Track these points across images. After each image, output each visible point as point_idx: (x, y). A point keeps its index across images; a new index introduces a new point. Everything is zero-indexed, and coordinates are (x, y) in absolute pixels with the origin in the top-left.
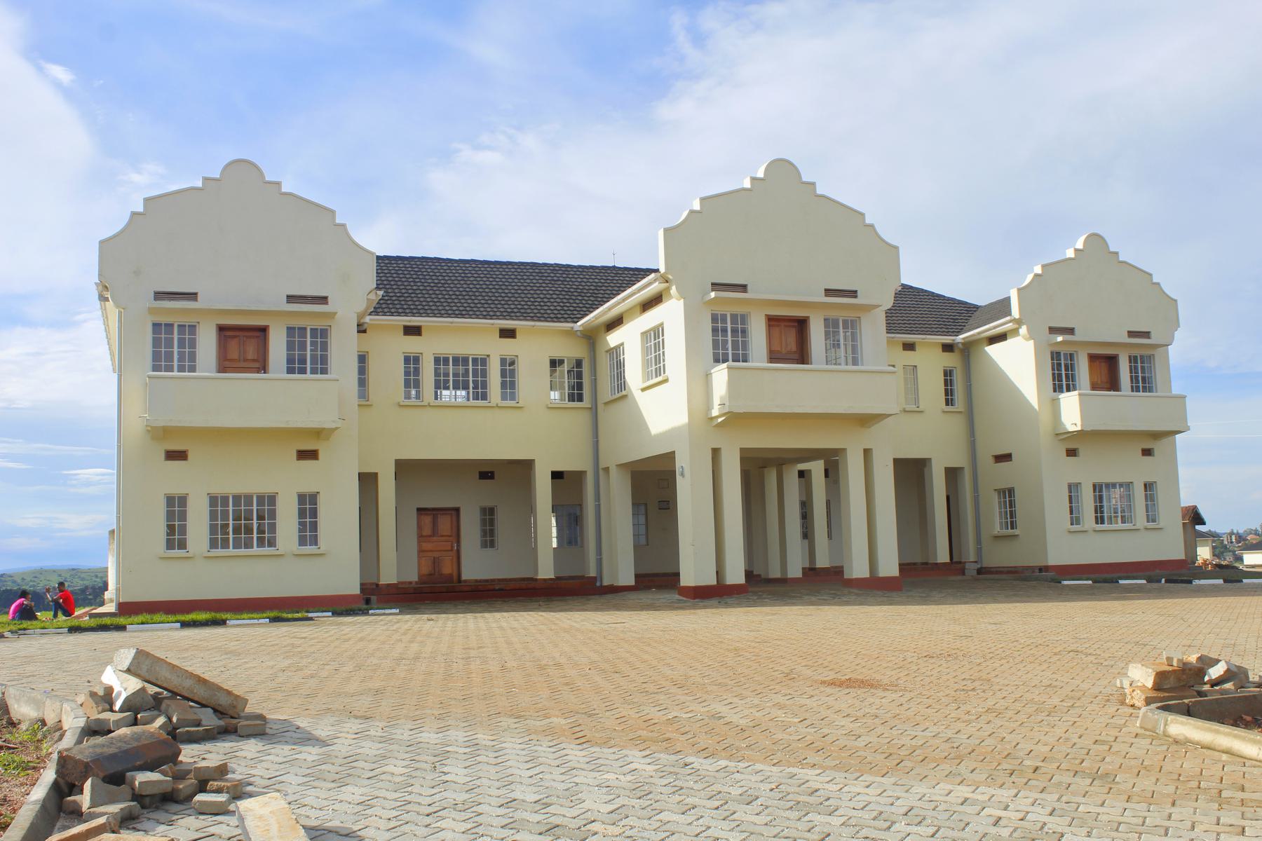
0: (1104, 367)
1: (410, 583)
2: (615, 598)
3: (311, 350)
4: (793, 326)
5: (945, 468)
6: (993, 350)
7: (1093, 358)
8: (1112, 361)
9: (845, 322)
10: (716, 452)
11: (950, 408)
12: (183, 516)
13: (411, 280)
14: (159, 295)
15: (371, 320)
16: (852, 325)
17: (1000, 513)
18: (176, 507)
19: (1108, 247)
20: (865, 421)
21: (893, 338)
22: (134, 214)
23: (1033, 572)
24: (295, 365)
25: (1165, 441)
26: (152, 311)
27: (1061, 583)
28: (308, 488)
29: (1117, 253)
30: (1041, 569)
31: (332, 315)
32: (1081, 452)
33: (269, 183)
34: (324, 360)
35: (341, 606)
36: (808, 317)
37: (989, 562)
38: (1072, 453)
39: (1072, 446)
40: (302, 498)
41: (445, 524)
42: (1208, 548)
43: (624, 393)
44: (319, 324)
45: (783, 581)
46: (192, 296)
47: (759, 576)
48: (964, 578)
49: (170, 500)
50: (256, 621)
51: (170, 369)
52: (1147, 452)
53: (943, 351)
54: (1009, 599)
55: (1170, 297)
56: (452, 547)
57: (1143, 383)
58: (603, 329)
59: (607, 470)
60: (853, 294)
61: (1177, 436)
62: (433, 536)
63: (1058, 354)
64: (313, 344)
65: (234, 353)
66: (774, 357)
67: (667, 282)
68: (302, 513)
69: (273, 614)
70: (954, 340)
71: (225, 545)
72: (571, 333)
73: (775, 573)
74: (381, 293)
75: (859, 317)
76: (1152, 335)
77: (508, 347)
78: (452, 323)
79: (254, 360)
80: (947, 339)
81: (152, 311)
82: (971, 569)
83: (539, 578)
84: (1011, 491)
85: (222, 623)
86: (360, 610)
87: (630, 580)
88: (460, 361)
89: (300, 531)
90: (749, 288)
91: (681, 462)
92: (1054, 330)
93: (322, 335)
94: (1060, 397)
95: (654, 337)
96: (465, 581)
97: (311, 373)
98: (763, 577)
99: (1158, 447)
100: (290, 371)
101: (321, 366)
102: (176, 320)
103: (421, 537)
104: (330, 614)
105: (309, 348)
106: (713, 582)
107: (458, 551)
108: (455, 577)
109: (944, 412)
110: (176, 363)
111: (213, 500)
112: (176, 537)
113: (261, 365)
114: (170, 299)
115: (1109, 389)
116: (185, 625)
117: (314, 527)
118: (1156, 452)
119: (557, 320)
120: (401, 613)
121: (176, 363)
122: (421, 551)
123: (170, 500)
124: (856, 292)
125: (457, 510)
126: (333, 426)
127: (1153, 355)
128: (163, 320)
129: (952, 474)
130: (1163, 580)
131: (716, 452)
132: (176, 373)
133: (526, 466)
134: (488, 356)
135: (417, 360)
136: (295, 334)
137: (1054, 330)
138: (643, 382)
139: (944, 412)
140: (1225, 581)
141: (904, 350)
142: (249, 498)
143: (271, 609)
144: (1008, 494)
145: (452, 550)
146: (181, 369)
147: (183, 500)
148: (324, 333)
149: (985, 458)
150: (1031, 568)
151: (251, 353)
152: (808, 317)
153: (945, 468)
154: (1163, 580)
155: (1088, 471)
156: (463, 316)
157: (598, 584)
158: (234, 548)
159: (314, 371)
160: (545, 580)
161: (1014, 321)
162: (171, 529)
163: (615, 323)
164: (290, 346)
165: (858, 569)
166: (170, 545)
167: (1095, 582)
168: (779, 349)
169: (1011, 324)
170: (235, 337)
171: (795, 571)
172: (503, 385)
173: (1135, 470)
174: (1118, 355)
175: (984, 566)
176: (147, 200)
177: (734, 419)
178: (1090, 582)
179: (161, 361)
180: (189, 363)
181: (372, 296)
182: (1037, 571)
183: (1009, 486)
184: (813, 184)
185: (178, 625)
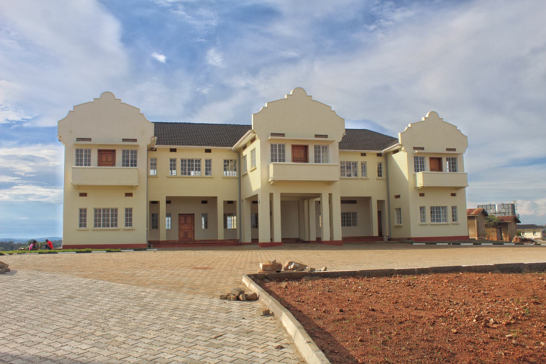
0: (437, 162)
1: (176, 241)
2: (246, 247)
3: (131, 158)
4: (303, 149)
5: (377, 200)
6: (395, 156)
7: (431, 159)
8: (439, 160)
9: (323, 147)
10: (271, 195)
11: (380, 178)
12: (85, 216)
13: (233, 131)
14: (78, 139)
15: (157, 147)
16: (325, 148)
17: (397, 217)
18: (83, 213)
19: (438, 116)
20: (329, 183)
21: (343, 151)
22: (70, 112)
23: (405, 240)
24: (126, 163)
25: (461, 190)
26: (75, 145)
27: (412, 244)
28: (129, 206)
29: (442, 119)
30: (408, 239)
31: (138, 146)
32: (425, 195)
33: (117, 99)
34: (136, 161)
35: (137, 248)
36: (308, 145)
37: (393, 236)
38: (422, 195)
39: (422, 193)
40: (127, 210)
41: (189, 220)
42: (540, 233)
43: (246, 173)
44: (134, 149)
45: (309, 242)
46: (90, 140)
47: (302, 240)
48: (383, 242)
49: (81, 210)
50: (101, 252)
51: (82, 165)
52: (453, 195)
53: (377, 156)
54: (364, 249)
55: (464, 135)
56: (192, 228)
57: (454, 168)
58: (242, 149)
59: (243, 200)
60: (326, 136)
61: (466, 188)
62: (185, 224)
63: (417, 157)
64: (131, 156)
65: (104, 159)
66: (295, 160)
67: (255, 133)
68: (127, 215)
69: (108, 249)
70: (381, 152)
71: (100, 226)
72: (231, 150)
73: (307, 240)
74: (156, 138)
75: (328, 145)
76: (457, 150)
77: (208, 156)
78: (187, 147)
79: (111, 162)
80: (378, 152)
81: (75, 145)
82: (386, 238)
83: (218, 239)
84: (400, 209)
85: (90, 252)
86: (144, 249)
87: (250, 241)
88: (349, 163)
89: (126, 221)
90: (285, 135)
91: (259, 198)
92: (415, 148)
93: (135, 153)
94: (417, 174)
95: (253, 151)
96: (196, 240)
97: (131, 166)
98: (304, 240)
99: (458, 193)
100: (123, 165)
101: (134, 164)
102: (84, 148)
103: (180, 224)
104: (133, 250)
105: (130, 157)
106: (269, 241)
107: (194, 229)
108: (193, 239)
109: (377, 179)
110: (130, 164)
111: (96, 210)
112: (83, 223)
113: (113, 164)
114: (82, 141)
115: (439, 171)
116: (77, 252)
117: (131, 220)
118: (457, 195)
119: (226, 146)
120: (158, 250)
121: (130, 164)
122: (180, 229)
123: (81, 210)
124: (327, 136)
125: (194, 214)
126: (136, 185)
127: (457, 157)
128: (80, 148)
129: (380, 203)
130: (451, 243)
131: (271, 195)
132: (83, 167)
133: (215, 199)
134: (201, 159)
135: (175, 160)
136: (125, 153)
137: (415, 148)
138: (251, 168)
139: (377, 179)
140: (493, 244)
141: (361, 156)
142: (108, 210)
143: (107, 248)
144: (399, 210)
145: (192, 229)
146: (86, 165)
147: (85, 210)
148: (136, 152)
149: (392, 197)
150: (405, 239)
151: (110, 159)
152: (308, 145)
153: (377, 200)
154: (451, 243)
155: (429, 202)
156: (191, 145)
157: (240, 242)
158: (103, 227)
159: (132, 166)
160: (220, 240)
161: (399, 145)
162: (81, 220)
163: (245, 147)
164: (123, 156)
165: (326, 237)
166: (81, 226)
167: (426, 244)
168: (297, 157)
169: (398, 146)
170: (105, 153)
171: (313, 238)
172: (362, 171)
173: (447, 201)
174: (442, 158)
175: (392, 237)
176: (74, 107)
177: (276, 183)
178: (425, 244)
179: (79, 162)
180: (88, 163)
181: (153, 139)
182: (407, 239)
183: (400, 207)
184: (311, 96)
185: (75, 252)
